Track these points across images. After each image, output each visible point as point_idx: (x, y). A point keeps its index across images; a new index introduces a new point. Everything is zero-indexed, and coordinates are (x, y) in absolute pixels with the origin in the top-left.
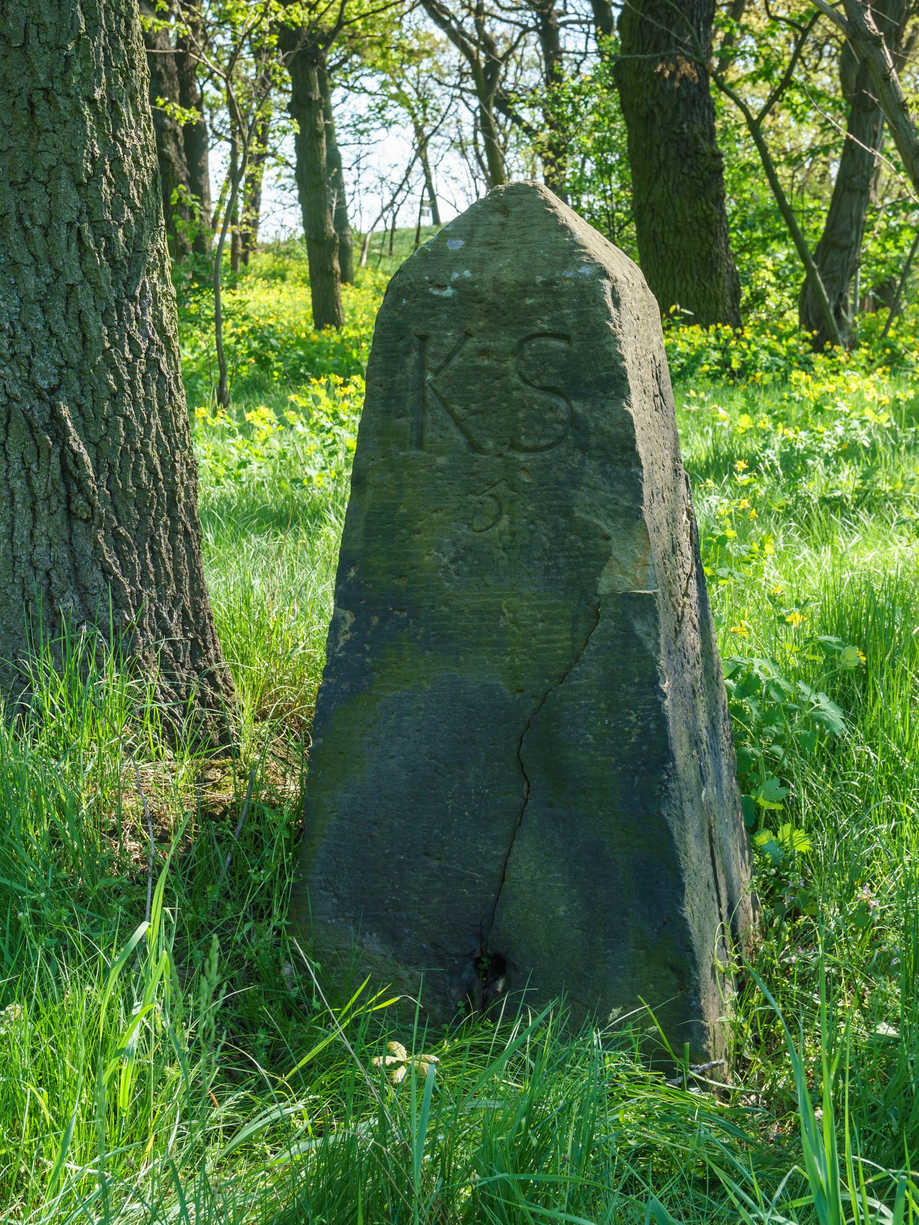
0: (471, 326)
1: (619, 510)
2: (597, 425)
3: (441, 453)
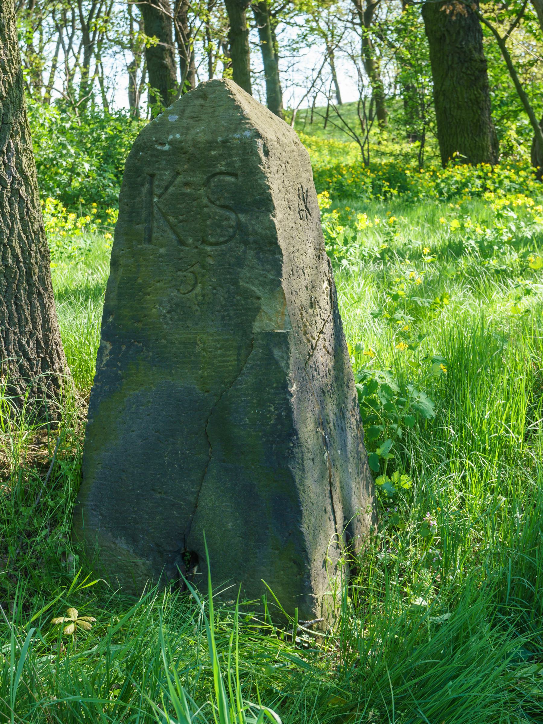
0: (179, 168)
1: (267, 281)
2: (253, 229)
3: (162, 246)
